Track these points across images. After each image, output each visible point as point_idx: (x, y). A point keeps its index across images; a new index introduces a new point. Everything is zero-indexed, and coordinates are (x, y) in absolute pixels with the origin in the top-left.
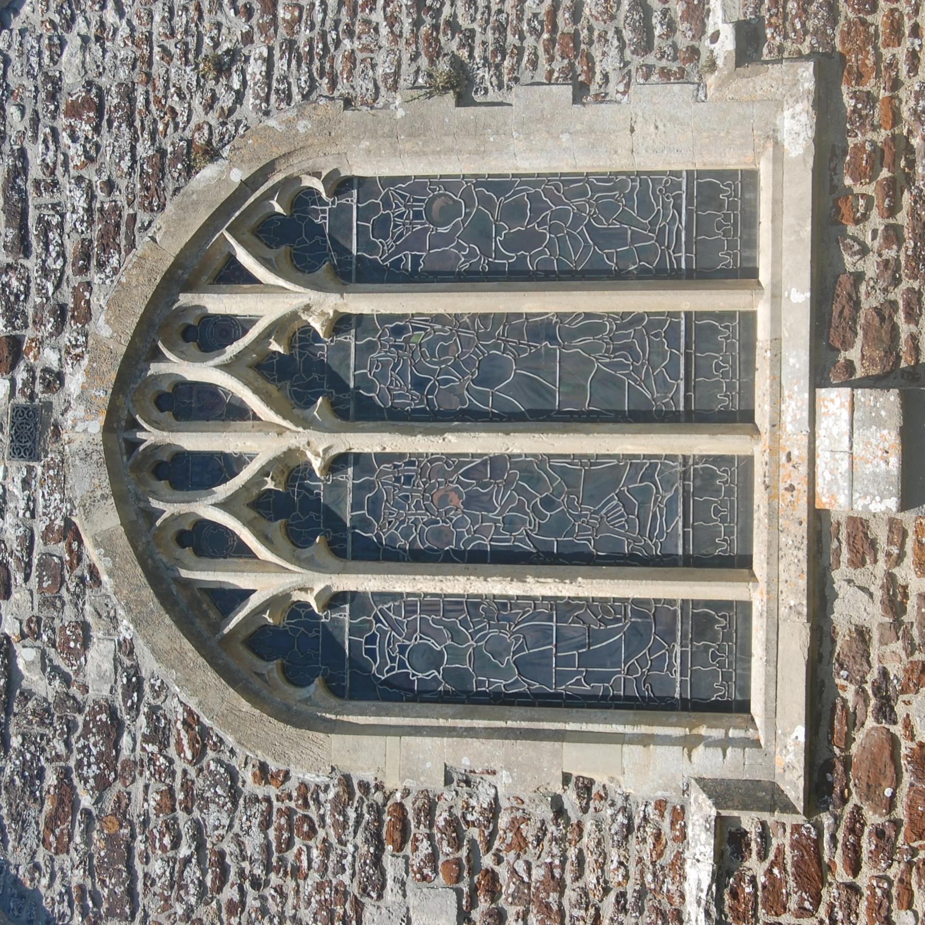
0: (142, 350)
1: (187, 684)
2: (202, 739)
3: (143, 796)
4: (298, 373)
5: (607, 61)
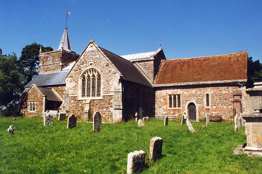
0: (94, 69)
1: (82, 72)
2: (80, 73)
3: (78, 71)
4: (94, 76)
5: (104, 90)
